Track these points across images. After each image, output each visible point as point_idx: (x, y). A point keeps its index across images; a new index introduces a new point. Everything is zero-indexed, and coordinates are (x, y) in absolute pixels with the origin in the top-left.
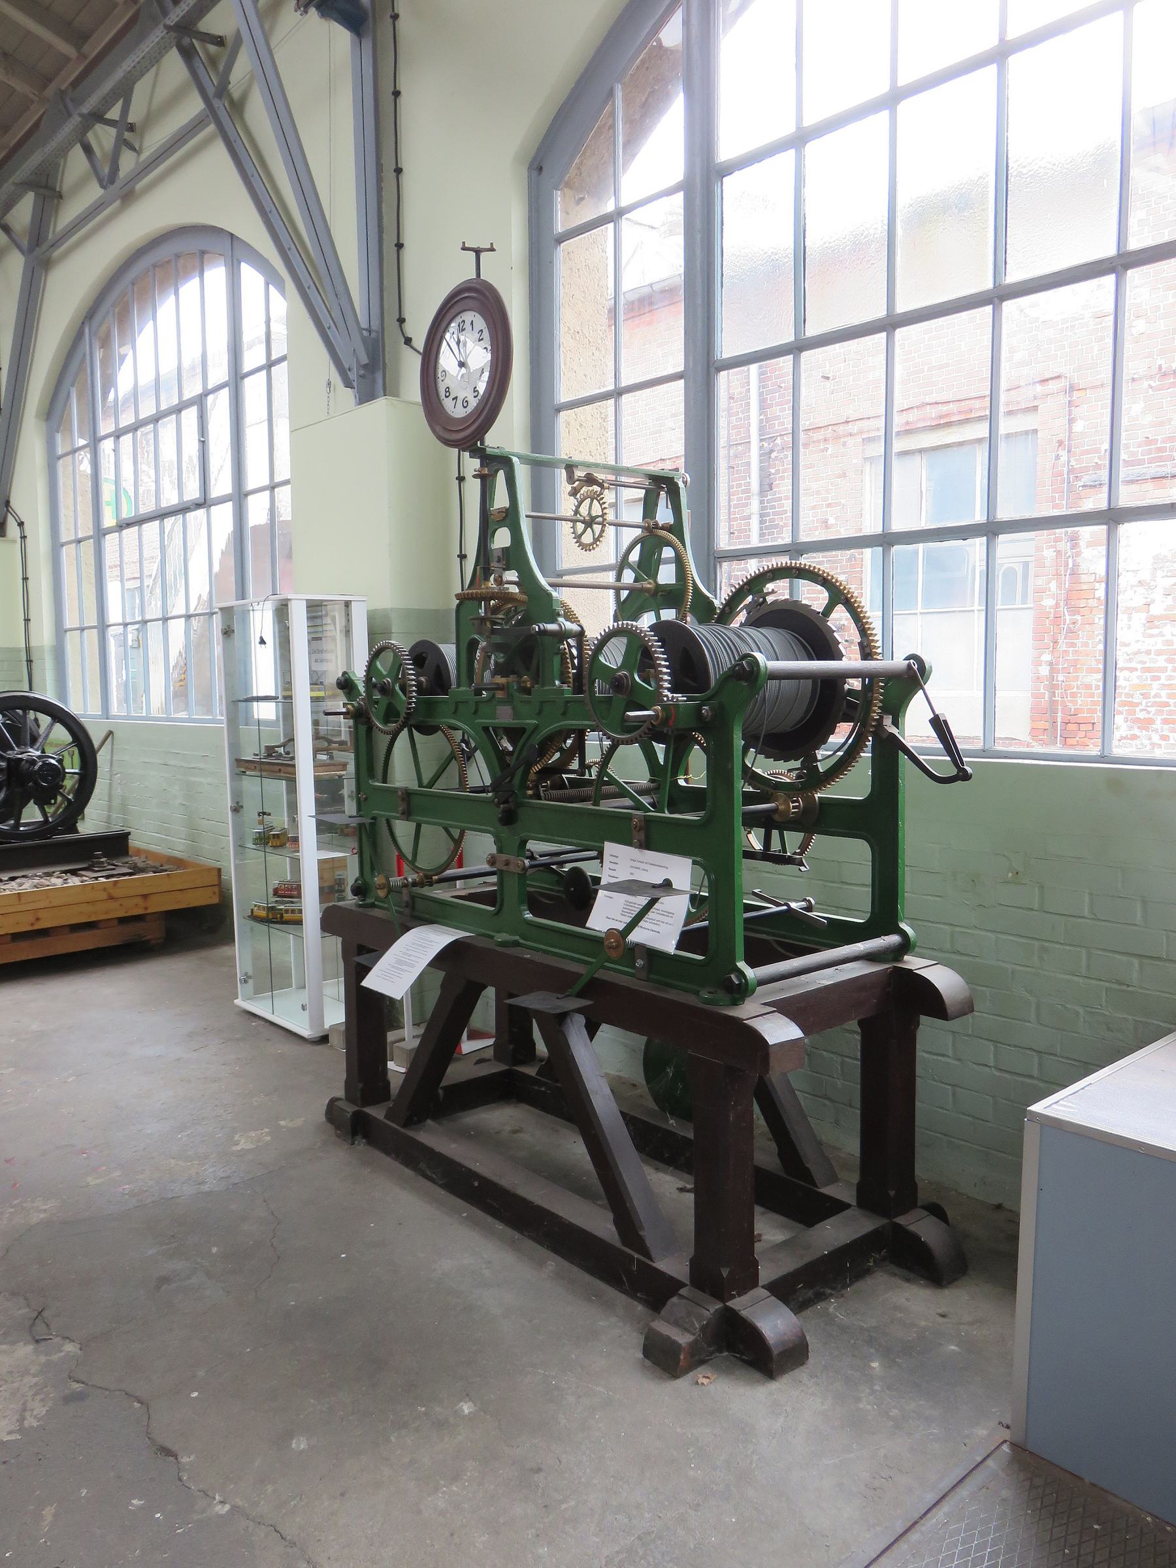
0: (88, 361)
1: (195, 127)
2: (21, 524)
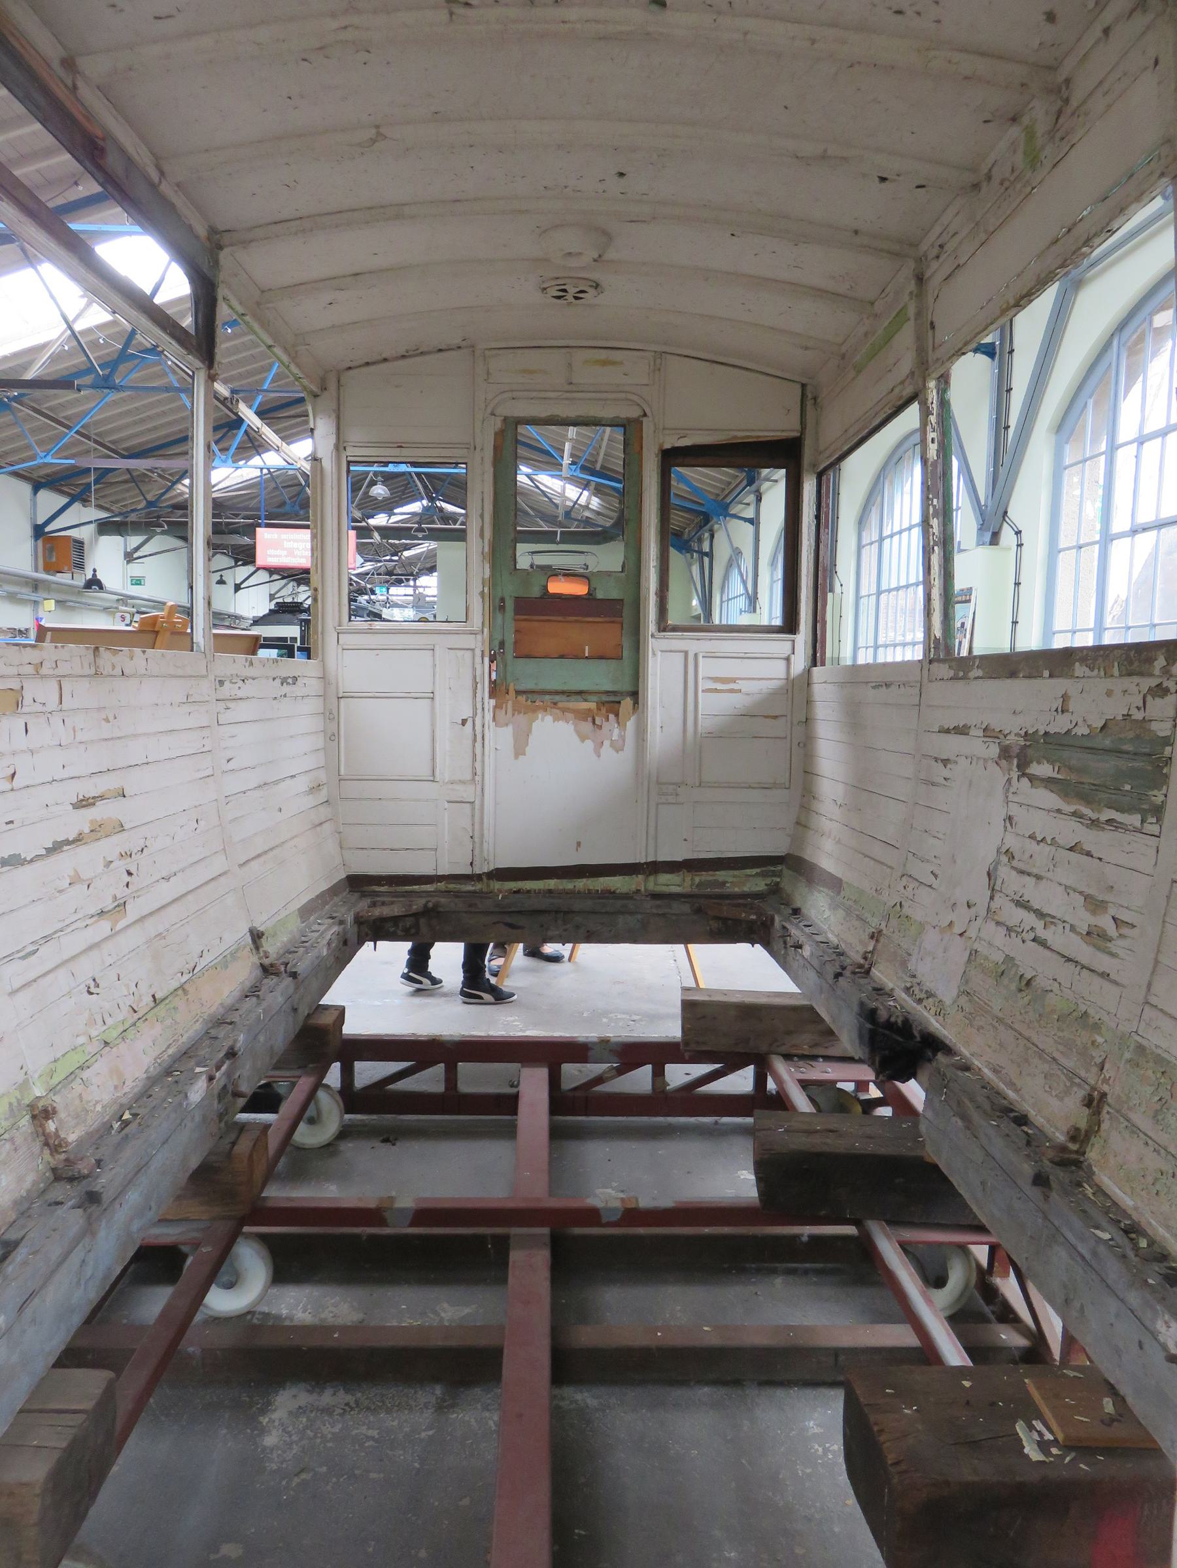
0: (1114, 372)
1: (1158, 216)
2: (1018, 533)
